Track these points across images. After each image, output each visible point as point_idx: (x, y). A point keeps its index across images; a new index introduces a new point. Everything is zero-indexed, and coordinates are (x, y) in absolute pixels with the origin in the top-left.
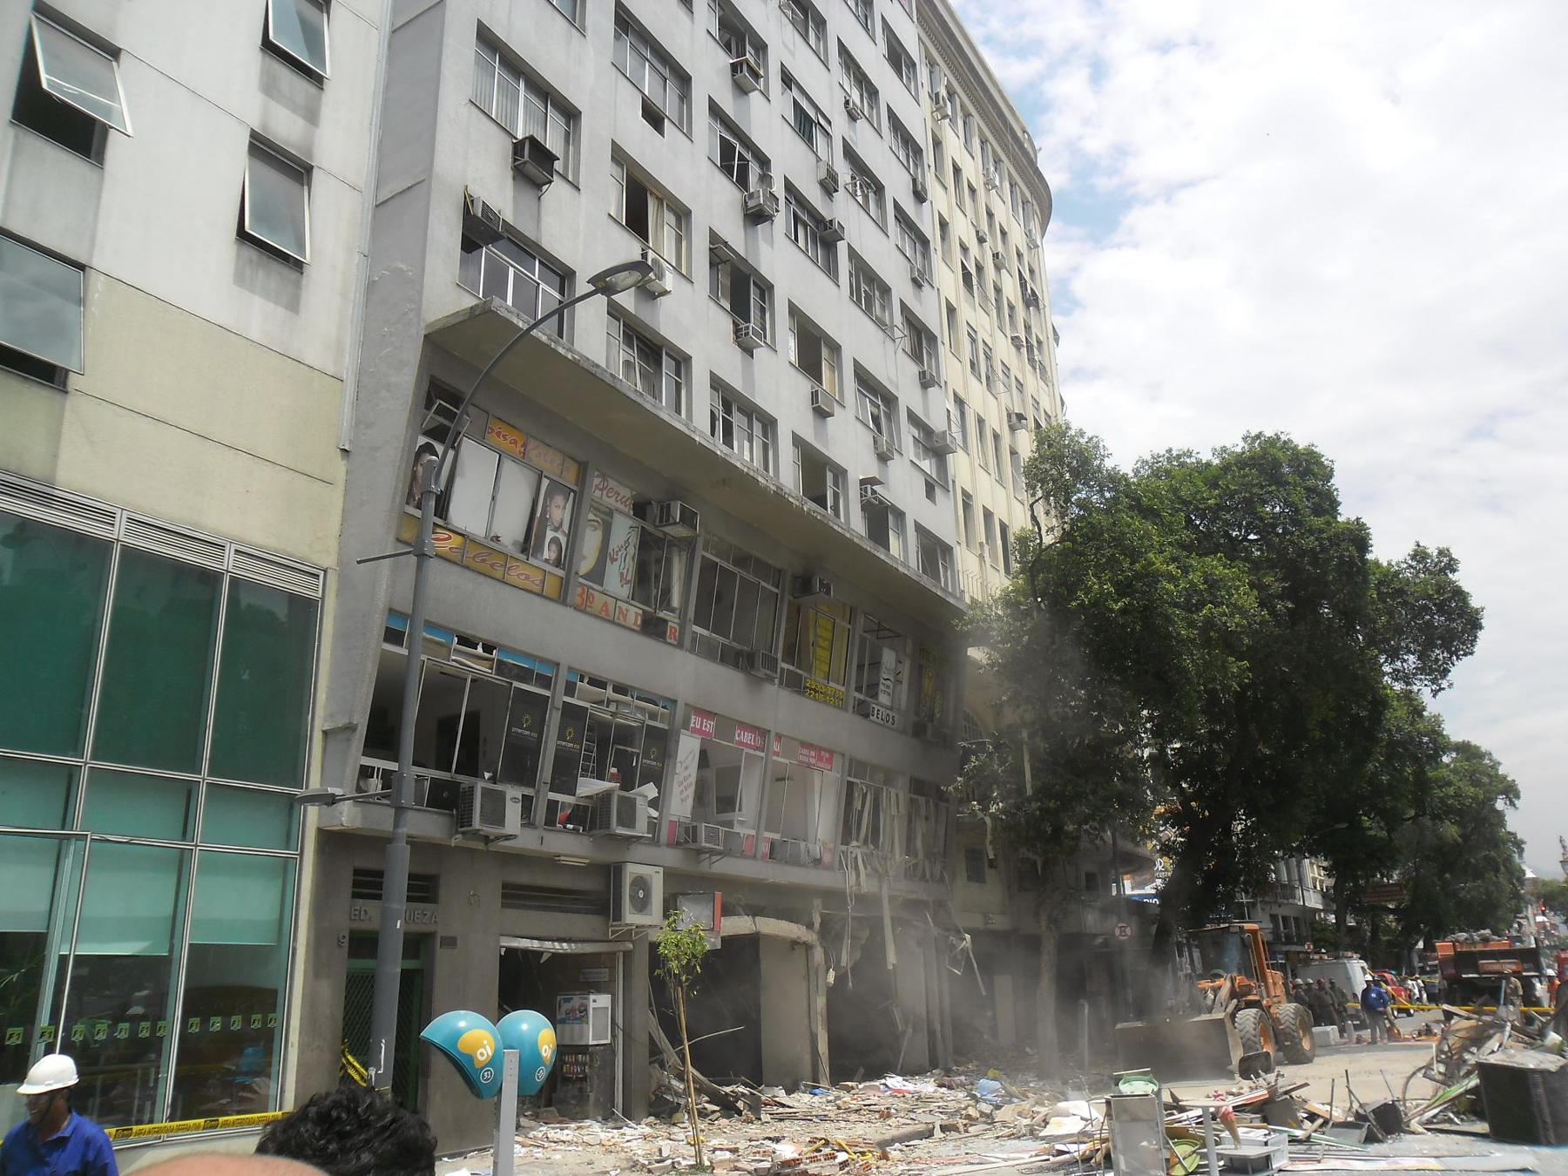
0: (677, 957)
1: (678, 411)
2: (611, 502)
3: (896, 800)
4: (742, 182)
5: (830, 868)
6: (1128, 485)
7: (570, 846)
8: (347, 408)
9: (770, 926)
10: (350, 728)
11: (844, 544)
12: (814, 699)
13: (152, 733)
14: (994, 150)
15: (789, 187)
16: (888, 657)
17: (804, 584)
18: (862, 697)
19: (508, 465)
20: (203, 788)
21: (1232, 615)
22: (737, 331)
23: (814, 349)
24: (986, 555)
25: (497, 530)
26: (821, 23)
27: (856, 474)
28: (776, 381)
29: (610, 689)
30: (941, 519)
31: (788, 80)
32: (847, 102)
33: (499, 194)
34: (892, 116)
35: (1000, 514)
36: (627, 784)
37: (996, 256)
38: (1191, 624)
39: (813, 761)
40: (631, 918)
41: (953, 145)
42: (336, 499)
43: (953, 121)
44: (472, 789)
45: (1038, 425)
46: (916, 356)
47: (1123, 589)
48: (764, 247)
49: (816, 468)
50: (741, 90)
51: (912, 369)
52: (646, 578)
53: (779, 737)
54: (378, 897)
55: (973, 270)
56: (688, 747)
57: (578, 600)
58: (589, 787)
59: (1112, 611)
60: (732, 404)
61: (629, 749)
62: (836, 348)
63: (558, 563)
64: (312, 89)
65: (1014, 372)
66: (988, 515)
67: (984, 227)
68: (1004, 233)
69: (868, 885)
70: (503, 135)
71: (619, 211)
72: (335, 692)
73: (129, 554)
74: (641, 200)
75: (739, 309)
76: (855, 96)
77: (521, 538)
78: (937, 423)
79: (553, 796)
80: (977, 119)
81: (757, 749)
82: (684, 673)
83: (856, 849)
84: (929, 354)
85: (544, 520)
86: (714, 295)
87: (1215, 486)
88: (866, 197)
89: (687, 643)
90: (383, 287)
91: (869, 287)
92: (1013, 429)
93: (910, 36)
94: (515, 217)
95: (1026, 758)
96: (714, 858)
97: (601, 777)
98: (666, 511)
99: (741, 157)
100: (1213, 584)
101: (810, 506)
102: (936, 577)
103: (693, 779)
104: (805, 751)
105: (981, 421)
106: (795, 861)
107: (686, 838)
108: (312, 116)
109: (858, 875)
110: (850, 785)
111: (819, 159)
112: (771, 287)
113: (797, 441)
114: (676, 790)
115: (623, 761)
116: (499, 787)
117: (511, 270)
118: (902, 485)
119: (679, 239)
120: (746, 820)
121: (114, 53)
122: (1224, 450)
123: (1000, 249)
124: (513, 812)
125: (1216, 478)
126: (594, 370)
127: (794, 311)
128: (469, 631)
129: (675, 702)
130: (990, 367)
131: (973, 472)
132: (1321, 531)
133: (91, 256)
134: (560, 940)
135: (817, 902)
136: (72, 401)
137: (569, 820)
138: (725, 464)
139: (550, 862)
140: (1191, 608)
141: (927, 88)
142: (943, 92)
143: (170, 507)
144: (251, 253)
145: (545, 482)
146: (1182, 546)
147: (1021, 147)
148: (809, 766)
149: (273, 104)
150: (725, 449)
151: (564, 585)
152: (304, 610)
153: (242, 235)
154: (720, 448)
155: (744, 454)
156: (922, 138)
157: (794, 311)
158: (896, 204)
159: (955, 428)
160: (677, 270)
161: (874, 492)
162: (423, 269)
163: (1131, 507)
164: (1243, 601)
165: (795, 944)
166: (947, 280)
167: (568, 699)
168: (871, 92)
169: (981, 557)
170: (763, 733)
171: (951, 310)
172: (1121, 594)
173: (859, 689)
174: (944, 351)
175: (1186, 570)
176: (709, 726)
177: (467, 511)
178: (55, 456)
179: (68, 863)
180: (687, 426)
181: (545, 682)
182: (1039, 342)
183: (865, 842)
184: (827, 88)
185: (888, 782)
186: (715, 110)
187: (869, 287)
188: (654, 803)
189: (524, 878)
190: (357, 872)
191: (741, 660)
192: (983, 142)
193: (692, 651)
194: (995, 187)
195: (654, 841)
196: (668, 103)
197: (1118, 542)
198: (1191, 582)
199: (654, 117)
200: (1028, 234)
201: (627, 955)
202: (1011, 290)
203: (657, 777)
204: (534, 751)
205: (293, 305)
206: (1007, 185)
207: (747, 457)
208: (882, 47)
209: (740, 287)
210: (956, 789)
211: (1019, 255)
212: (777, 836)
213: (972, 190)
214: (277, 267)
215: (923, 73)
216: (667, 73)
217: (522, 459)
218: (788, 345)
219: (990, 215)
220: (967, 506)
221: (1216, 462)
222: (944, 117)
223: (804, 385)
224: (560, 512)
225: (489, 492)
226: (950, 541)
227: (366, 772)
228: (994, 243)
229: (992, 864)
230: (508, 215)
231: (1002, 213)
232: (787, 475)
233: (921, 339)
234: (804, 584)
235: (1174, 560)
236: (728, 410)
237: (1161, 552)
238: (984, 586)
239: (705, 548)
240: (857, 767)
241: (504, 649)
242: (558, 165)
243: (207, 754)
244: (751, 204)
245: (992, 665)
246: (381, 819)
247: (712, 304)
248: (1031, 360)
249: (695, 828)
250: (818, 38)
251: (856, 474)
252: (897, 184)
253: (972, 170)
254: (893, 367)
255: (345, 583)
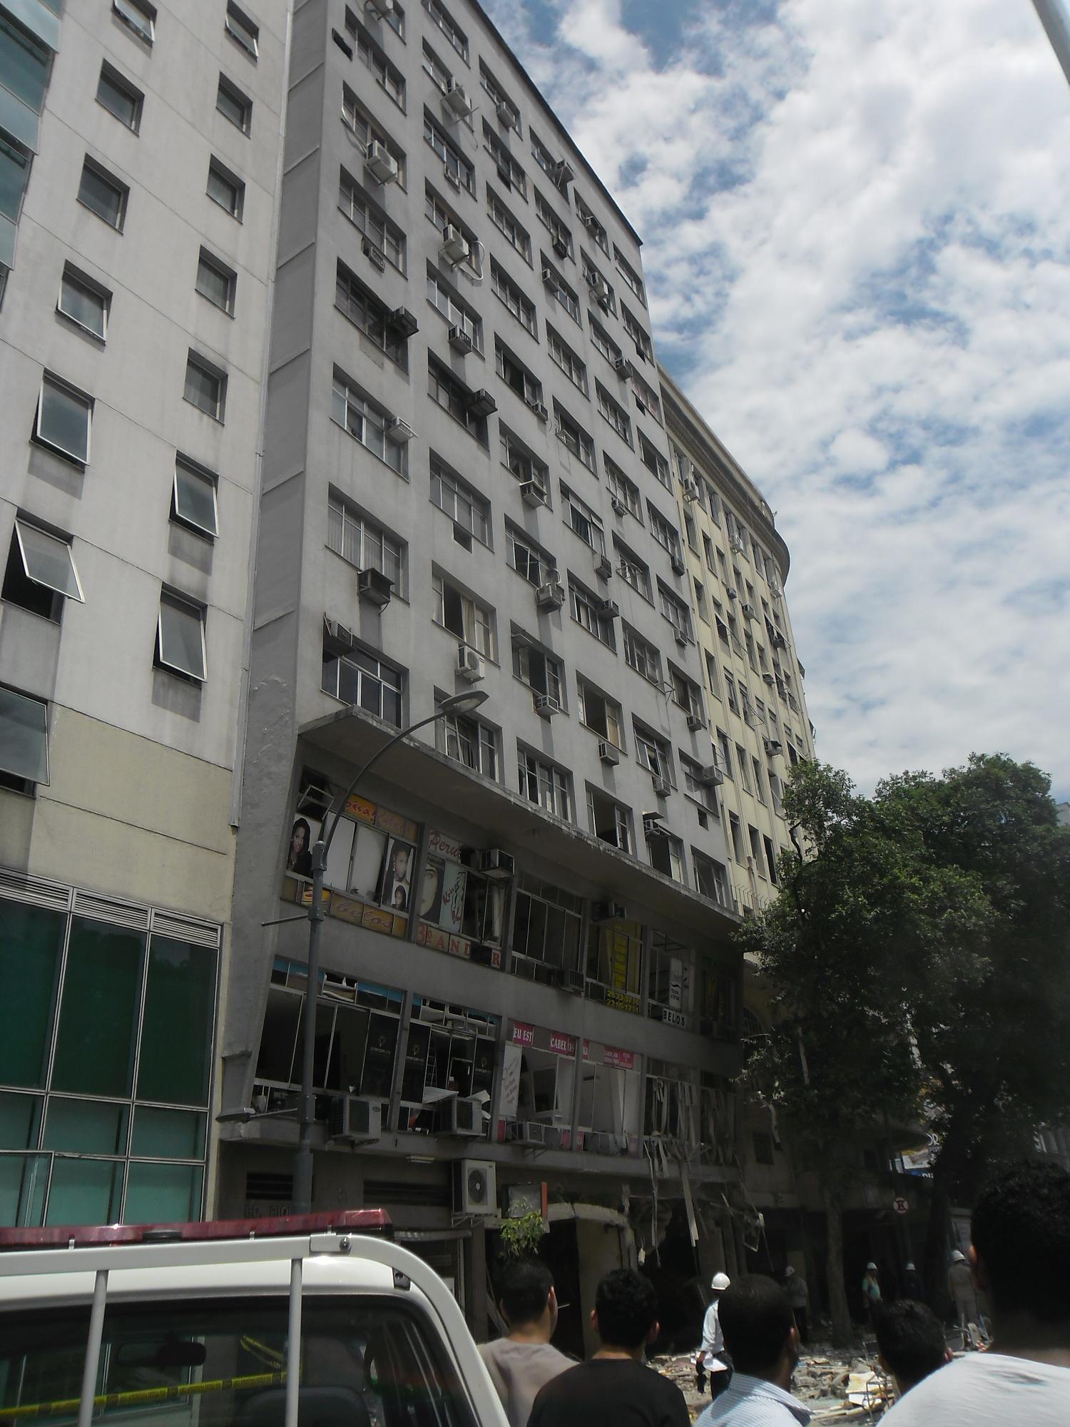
0: (518, 1241)
1: (493, 777)
2: (442, 854)
3: (690, 1094)
4: (534, 580)
5: (635, 1156)
6: (872, 810)
7: (420, 1148)
8: (237, 795)
9: (587, 1211)
10: (246, 1055)
11: (636, 875)
12: (616, 1007)
13: (95, 1065)
14: (736, 519)
15: (572, 578)
16: (676, 966)
17: (602, 910)
18: (654, 1003)
19: (363, 831)
20: (133, 1110)
21: (970, 918)
22: (537, 702)
23: (600, 709)
24: (754, 867)
25: (355, 884)
26: (589, 442)
27: (639, 811)
28: (572, 744)
29: (447, 1009)
30: (714, 842)
31: (566, 491)
32: (614, 503)
33: (348, 616)
34: (651, 507)
35: (764, 830)
36: (464, 1092)
37: (745, 608)
38: (935, 927)
39: (616, 1062)
40: (471, 1208)
41: (703, 520)
42: (228, 866)
43: (701, 501)
44: (342, 1101)
45: (792, 752)
46: (683, 704)
47: (875, 899)
48: (554, 632)
49: (607, 810)
50: (529, 506)
51: (681, 716)
52: (474, 915)
53: (587, 1042)
54: (289, 1197)
55: (726, 623)
56: (512, 1055)
57: (420, 937)
58: (433, 1095)
59: (866, 919)
60: (539, 766)
61: (466, 1062)
62: (617, 706)
63: (402, 907)
64: (206, 546)
65: (768, 705)
66: (753, 832)
67: (733, 585)
68: (750, 588)
69: (668, 1171)
70: (350, 569)
71: (439, 616)
72: (232, 1024)
73: (78, 921)
74: (457, 605)
75: (537, 684)
76: (620, 496)
77: (373, 889)
78: (705, 760)
79: (404, 1104)
80: (721, 496)
81: (568, 1053)
82: (509, 994)
83: (657, 1138)
84: (694, 701)
85: (391, 873)
86: (517, 675)
87: (948, 804)
88: (634, 578)
89: (508, 967)
90: (260, 698)
91: (641, 652)
92: (770, 755)
93: (660, 439)
94: (362, 632)
95: (802, 1050)
96: (538, 1152)
97: (441, 1085)
98: (487, 857)
99: (532, 559)
100: (951, 891)
101: (604, 845)
102: (713, 896)
103: (517, 1083)
104: (609, 1054)
105: (741, 751)
106: (604, 1151)
107: (512, 1134)
108: (205, 567)
109: (660, 1162)
110: (650, 1081)
111: (594, 552)
112: (561, 662)
113: (590, 787)
114: (504, 1092)
115: (459, 1071)
116: (363, 1099)
117: (360, 674)
118: (680, 818)
119: (487, 633)
120: (561, 1116)
121: (68, 539)
122: (953, 771)
123: (748, 602)
124: (375, 1120)
125: (948, 797)
126: (430, 753)
127: (581, 679)
128: (336, 969)
129: (499, 1018)
130: (747, 704)
131: (738, 795)
132: (1044, 838)
133: (53, 693)
134: (412, 1230)
135: (626, 1188)
136: (40, 805)
137: (417, 1124)
138: (535, 818)
139: (402, 1162)
140: (933, 913)
141: (677, 476)
142: (691, 479)
143: (106, 881)
144: (163, 677)
145: (391, 842)
146: (924, 859)
147: (760, 515)
148: (613, 1066)
149: (178, 562)
150: (533, 805)
151: (409, 924)
152: (204, 959)
153: (157, 664)
154: (531, 807)
155: (547, 807)
156: (677, 521)
157: (581, 679)
158: (659, 580)
159: (719, 760)
160: (487, 657)
161: (656, 825)
162: (295, 682)
163: (876, 829)
164: (977, 906)
165: (608, 1226)
166: (705, 634)
167: (414, 1021)
168: (631, 489)
169: (750, 869)
170: (573, 1040)
171: (710, 659)
172: (873, 905)
173: (652, 995)
174: (706, 694)
175: (926, 880)
176: (528, 1036)
177: (334, 875)
178: (27, 850)
179: (33, 1176)
180: (504, 790)
181: (395, 1007)
182: (787, 677)
183: (665, 1133)
184: (596, 493)
185: (682, 1076)
186: (510, 525)
187: (641, 652)
188: (487, 1107)
189: (382, 1176)
190: (251, 1176)
191: (552, 977)
192: (728, 514)
193: (512, 972)
194: (740, 550)
195: (488, 1139)
196: (473, 527)
197: (866, 860)
198: (932, 892)
199: (463, 537)
200: (771, 586)
201: (467, 1241)
202: (760, 635)
203: (487, 1083)
204: (388, 1064)
205: (195, 715)
206: (750, 548)
207: (549, 809)
208: (639, 453)
209: (537, 665)
210: (741, 1080)
211: (765, 604)
212: (588, 1130)
213: (721, 555)
214: (182, 686)
215: (673, 466)
216: (470, 500)
217: (374, 826)
218: (579, 710)
219: (737, 574)
220: (735, 826)
221: (947, 781)
222: (694, 498)
223: (592, 741)
224: (404, 865)
225: (352, 857)
226: (721, 859)
227: (257, 1090)
228: (743, 598)
229: (778, 1147)
230: (357, 632)
231: (747, 570)
232: (583, 820)
233: (687, 691)
234: (602, 910)
235: (916, 872)
236: (532, 768)
237: (905, 866)
238: (755, 899)
239: (520, 886)
240: (655, 1065)
241: (363, 982)
242: (392, 588)
243: (135, 1081)
244: (542, 597)
245: (766, 970)
246: (286, 1132)
247: (515, 683)
248: (781, 694)
249: (521, 1127)
250: (587, 454)
251: (639, 811)
252: (658, 564)
253: (719, 539)
254: (666, 717)
255: (236, 932)
